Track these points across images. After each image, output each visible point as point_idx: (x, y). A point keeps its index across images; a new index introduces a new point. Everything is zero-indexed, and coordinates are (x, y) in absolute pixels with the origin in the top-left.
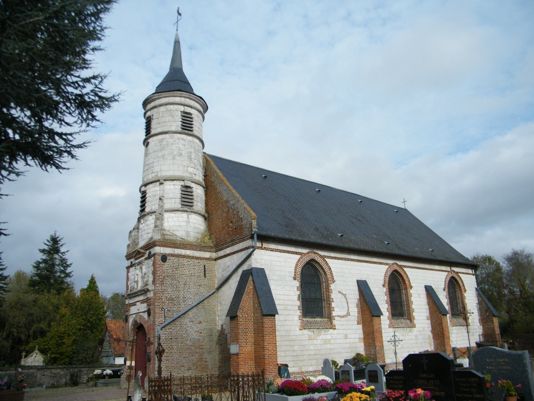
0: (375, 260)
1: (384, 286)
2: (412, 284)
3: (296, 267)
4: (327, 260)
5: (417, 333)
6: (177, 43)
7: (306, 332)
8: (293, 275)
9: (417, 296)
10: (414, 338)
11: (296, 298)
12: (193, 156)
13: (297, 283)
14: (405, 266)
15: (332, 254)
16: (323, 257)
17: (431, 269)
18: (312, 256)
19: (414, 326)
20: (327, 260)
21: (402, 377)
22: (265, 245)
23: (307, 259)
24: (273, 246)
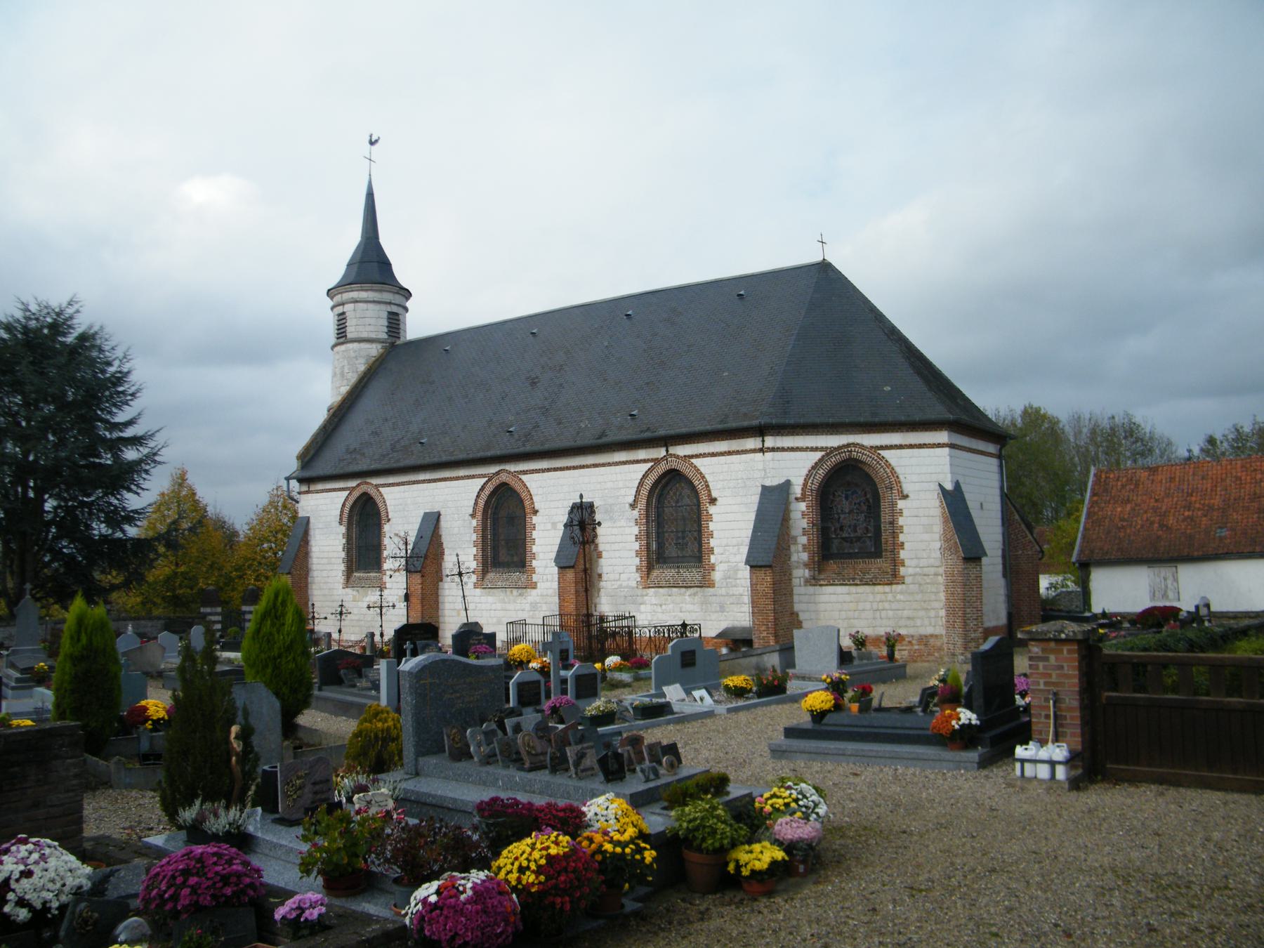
0: (422, 476)
1: (473, 516)
2: (537, 506)
3: (708, 486)
4: (524, 477)
5: (538, 599)
6: (370, 196)
7: (349, 590)
8: (471, 511)
9: (549, 526)
10: (527, 607)
11: (341, 548)
12: (346, 370)
13: (343, 529)
14: (525, 472)
15: (391, 480)
16: (377, 486)
17: (595, 466)
18: (364, 488)
19: (534, 586)
20: (524, 477)
21: (219, 610)
22: (313, 487)
23: (356, 494)
24: (320, 486)
